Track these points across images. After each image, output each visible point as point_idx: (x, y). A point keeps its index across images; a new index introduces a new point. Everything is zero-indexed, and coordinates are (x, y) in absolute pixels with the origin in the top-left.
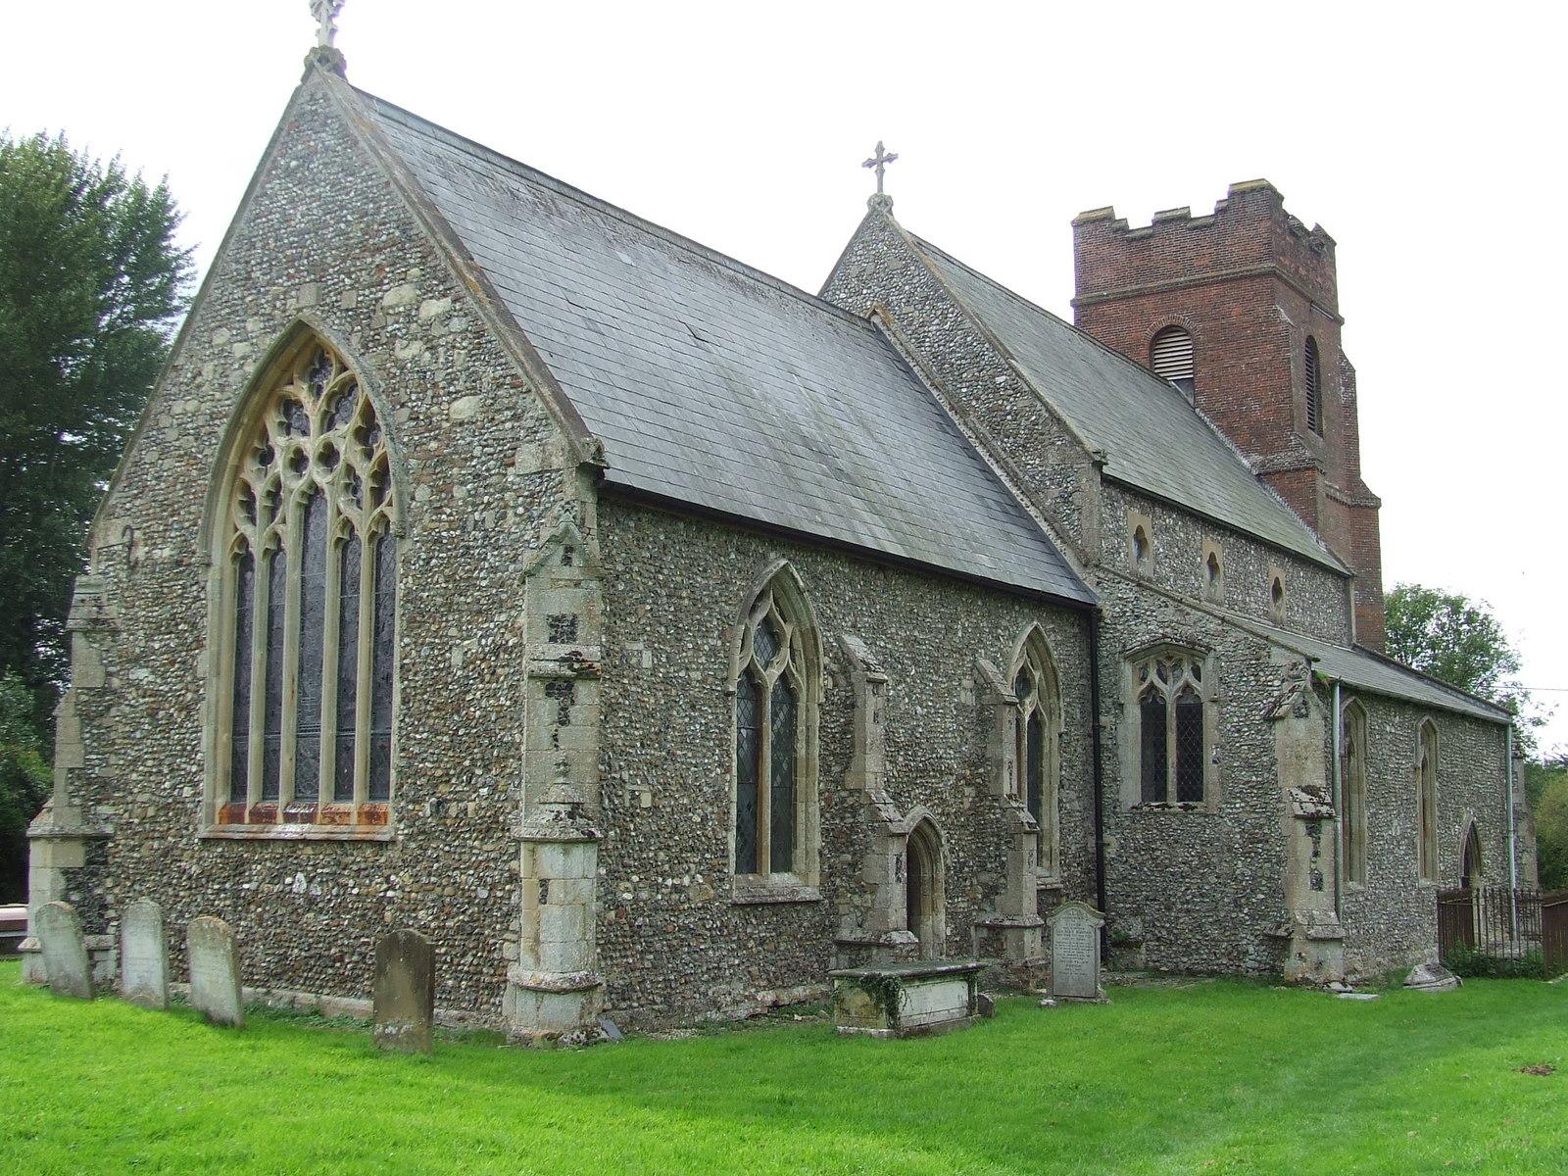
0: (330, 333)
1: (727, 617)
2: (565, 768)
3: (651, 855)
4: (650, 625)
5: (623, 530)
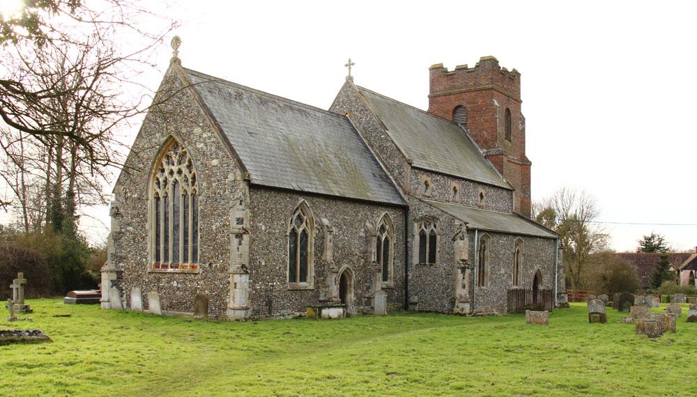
2: (241, 256)
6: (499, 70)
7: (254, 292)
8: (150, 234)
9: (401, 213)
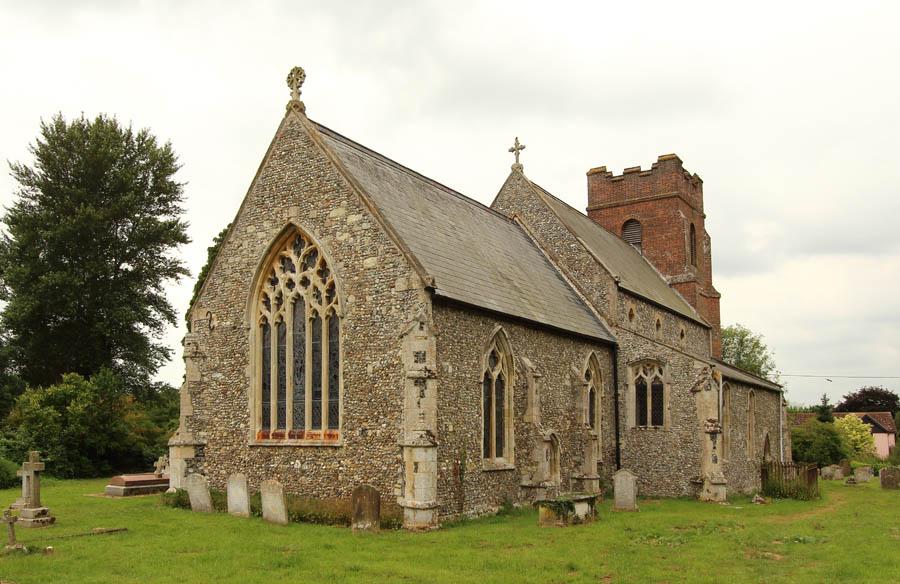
0: (306, 228)
8: (252, 383)
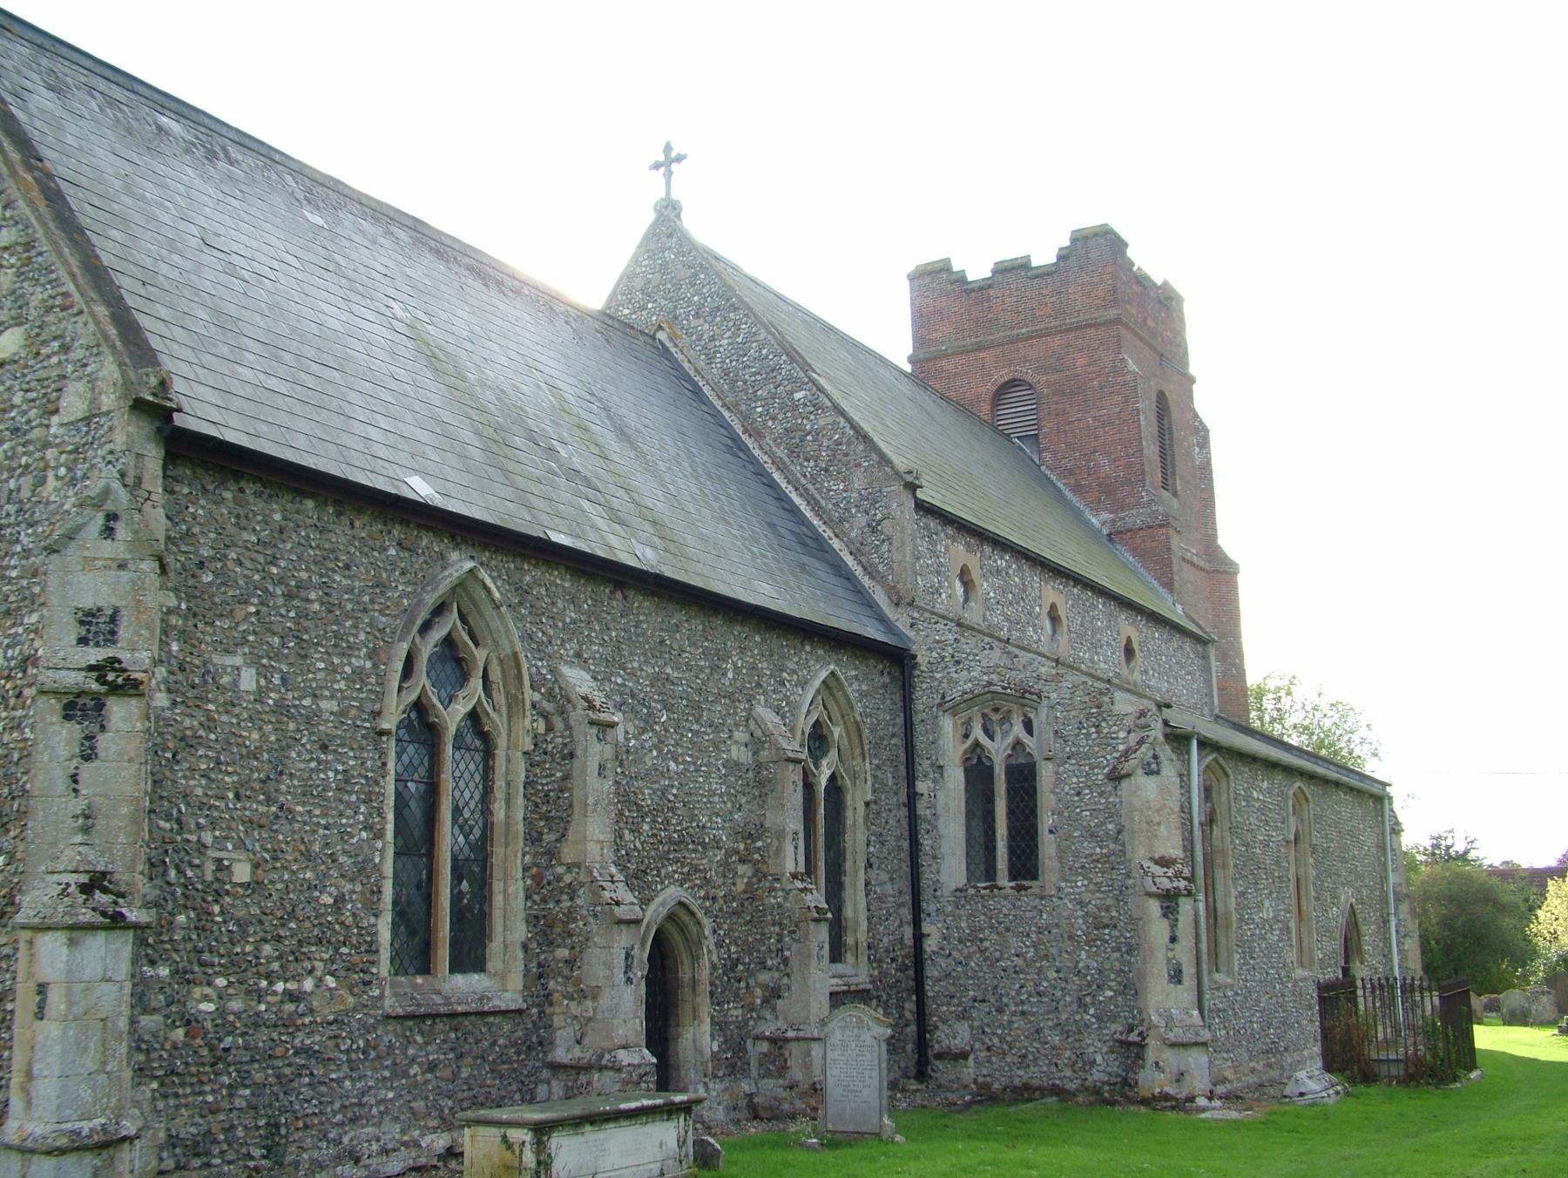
1: (382, 631)
3: (248, 948)
4: (255, 633)
5: (215, 503)
6: (1131, 270)
7: (179, 1034)
9: (886, 679)
